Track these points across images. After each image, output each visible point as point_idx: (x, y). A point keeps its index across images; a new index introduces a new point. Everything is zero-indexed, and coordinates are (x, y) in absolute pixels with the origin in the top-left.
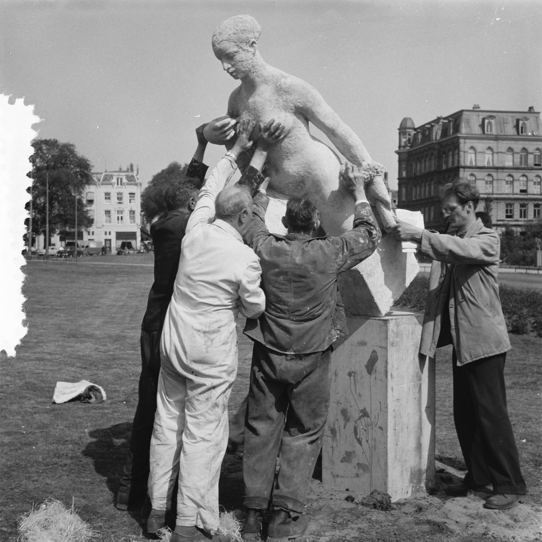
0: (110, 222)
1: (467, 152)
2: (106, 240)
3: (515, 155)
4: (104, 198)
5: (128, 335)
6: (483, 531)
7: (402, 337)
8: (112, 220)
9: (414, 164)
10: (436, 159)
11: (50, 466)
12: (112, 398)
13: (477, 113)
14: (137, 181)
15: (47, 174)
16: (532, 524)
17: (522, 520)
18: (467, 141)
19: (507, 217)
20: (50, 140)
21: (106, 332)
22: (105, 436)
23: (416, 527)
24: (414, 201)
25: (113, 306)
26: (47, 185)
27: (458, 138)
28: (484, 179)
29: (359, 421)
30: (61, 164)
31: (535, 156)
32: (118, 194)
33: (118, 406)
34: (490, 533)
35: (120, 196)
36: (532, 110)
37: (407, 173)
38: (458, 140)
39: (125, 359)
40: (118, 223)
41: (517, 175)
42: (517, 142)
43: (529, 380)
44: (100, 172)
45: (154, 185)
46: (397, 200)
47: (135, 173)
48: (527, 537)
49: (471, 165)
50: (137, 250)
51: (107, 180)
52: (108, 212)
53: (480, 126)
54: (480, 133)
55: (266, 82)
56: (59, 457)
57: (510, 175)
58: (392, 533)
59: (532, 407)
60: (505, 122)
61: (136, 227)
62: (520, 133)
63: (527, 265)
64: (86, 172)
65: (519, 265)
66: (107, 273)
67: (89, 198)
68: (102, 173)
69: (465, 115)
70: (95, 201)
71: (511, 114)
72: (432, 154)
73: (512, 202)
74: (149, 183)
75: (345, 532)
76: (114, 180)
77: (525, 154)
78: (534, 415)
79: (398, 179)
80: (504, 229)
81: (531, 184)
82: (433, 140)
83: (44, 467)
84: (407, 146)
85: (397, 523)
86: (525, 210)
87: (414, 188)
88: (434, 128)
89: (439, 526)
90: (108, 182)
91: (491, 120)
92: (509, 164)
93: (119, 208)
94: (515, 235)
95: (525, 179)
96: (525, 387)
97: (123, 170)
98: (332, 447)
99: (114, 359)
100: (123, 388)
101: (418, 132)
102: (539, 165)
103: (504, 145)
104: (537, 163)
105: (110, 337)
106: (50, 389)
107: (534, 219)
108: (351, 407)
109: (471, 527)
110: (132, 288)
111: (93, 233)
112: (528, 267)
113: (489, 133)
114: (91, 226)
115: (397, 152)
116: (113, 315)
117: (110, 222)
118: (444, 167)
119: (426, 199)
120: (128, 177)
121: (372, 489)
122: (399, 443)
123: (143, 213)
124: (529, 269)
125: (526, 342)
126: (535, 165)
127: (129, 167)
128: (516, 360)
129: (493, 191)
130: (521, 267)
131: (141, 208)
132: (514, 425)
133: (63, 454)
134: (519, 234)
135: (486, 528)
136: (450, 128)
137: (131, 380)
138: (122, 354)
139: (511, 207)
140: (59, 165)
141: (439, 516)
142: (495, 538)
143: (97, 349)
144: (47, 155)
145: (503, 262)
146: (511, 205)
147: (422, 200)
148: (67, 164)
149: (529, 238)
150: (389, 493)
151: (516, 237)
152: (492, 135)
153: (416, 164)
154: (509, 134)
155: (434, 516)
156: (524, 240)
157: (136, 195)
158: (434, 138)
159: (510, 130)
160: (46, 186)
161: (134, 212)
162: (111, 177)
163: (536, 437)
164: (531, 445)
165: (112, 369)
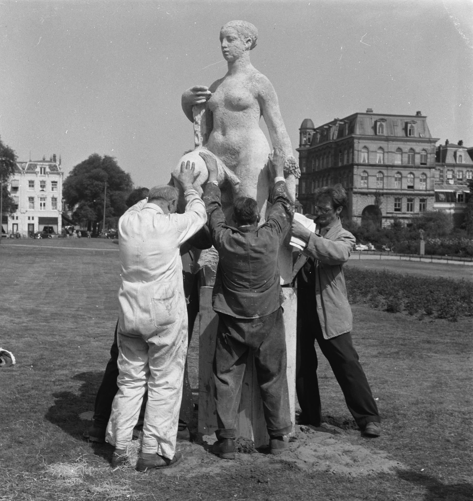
0: (33, 208)
1: (361, 151)
2: (29, 224)
3: (404, 155)
4: (28, 186)
5: (42, 309)
6: (324, 468)
8: (35, 206)
9: (313, 161)
12: (21, 363)
13: (370, 116)
14: (59, 171)
16: (368, 463)
17: (360, 460)
18: (361, 141)
19: (396, 210)
21: (22, 306)
22: (11, 394)
23: (270, 465)
25: (32, 284)
27: (353, 138)
28: (376, 176)
31: (422, 155)
32: (41, 182)
33: (25, 369)
34: (332, 470)
35: (43, 184)
36: (419, 115)
37: (307, 169)
38: (353, 140)
39: (37, 330)
40: (41, 209)
41: (405, 172)
42: (405, 143)
43: (393, 350)
45: (75, 175)
48: (362, 473)
49: (380, 164)
50: (58, 234)
51: (31, 169)
52: (31, 199)
53: (372, 128)
54: (372, 134)
57: (398, 173)
58: (249, 470)
59: (391, 372)
60: (395, 125)
62: (408, 135)
63: (412, 253)
64: (12, 161)
65: (404, 253)
66: (28, 255)
67: (14, 186)
68: (26, 163)
69: (359, 118)
70: (19, 189)
71: (401, 118)
73: (400, 197)
74: (70, 173)
75: (209, 469)
76: (38, 169)
77: (413, 154)
78: (390, 379)
80: (392, 221)
81: (417, 181)
82: (330, 140)
85: (255, 463)
86: (411, 204)
87: (313, 182)
88: (331, 129)
89: (289, 465)
90: (32, 171)
91: (383, 123)
92: (398, 162)
93: (42, 195)
94: (402, 227)
95: (412, 176)
96: (388, 356)
98: (207, 401)
99: (27, 330)
100: (31, 355)
101: (317, 132)
102: (425, 164)
103: (394, 146)
104: (423, 162)
105: (25, 310)
107: (420, 213)
109: (316, 465)
110: (49, 269)
111: (17, 218)
112: (411, 255)
113: (381, 134)
114: (15, 212)
115: (298, 150)
116: (29, 292)
117: (33, 208)
118: (340, 164)
120: (50, 167)
123: (64, 200)
124: (413, 257)
125: (398, 319)
126: (422, 164)
127: (52, 157)
128: (386, 334)
129: (383, 186)
130: (406, 255)
131: (63, 196)
132: (371, 386)
134: (406, 225)
135: (328, 466)
136: (346, 129)
137: (40, 348)
138: (35, 325)
139: (399, 201)
141: (291, 457)
142: (334, 474)
143: (12, 320)
145: (390, 251)
146: (399, 199)
149: (414, 229)
151: (403, 228)
152: (384, 136)
153: (315, 161)
154: (399, 136)
155: (287, 457)
156: (410, 231)
158: (331, 139)
159: (400, 132)
162: (35, 166)
163: (388, 396)
164: (382, 403)
165: (24, 338)
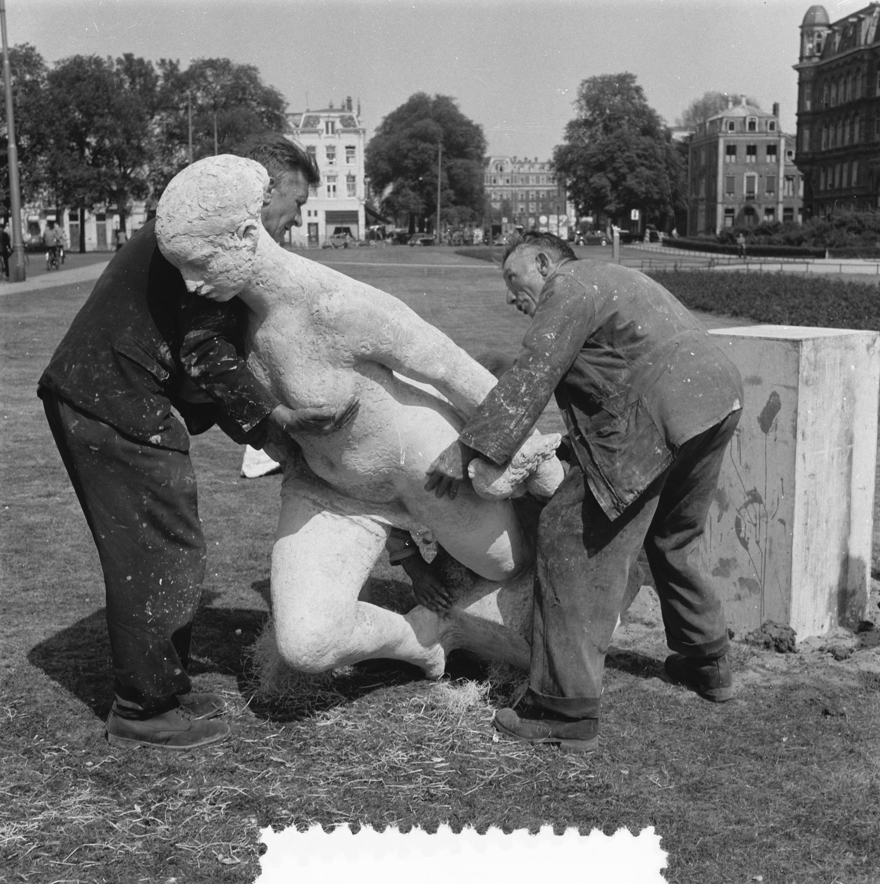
7: (824, 369)
9: (826, 88)
10: (865, 78)
11: (245, 572)
14: (359, 127)
15: (215, 116)
20: (218, 60)
24: (824, 153)
26: (216, 135)
29: (744, 510)
30: (236, 98)
35: (331, 152)
37: (813, 105)
40: (329, 196)
44: (296, 111)
46: (794, 152)
47: (354, 113)
50: (359, 240)
55: (287, 299)
56: (256, 559)
61: (358, 203)
64: (276, 112)
68: (301, 114)
72: (859, 70)
76: (322, 125)
79: (798, 114)
82: (860, 44)
83: (236, 574)
84: (815, 56)
87: (824, 130)
88: (863, 23)
90: (312, 129)
93: (331, 171)
97: (335, 107)
101: (834, 32)
106: (237, 456)
108: (731, 485)
115: (796, 68)
119: (845, 149)
121: (764, 620)
122: (812, 547)
123: (368, 179)
127: (345, 102)
133: (263, 554)
140: (233, 102)
144: (214, 85)
147: (838, 150)
148: (245, 99)
150: (793, 625)
153: (830, 88)
157: (357, 150)
158: (863, 42)
160: (213, 137)
161: (354, 177)
162: (317, 120)
